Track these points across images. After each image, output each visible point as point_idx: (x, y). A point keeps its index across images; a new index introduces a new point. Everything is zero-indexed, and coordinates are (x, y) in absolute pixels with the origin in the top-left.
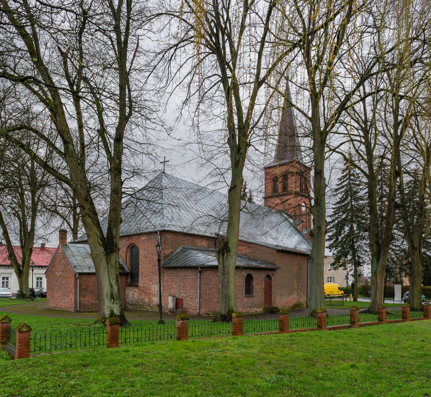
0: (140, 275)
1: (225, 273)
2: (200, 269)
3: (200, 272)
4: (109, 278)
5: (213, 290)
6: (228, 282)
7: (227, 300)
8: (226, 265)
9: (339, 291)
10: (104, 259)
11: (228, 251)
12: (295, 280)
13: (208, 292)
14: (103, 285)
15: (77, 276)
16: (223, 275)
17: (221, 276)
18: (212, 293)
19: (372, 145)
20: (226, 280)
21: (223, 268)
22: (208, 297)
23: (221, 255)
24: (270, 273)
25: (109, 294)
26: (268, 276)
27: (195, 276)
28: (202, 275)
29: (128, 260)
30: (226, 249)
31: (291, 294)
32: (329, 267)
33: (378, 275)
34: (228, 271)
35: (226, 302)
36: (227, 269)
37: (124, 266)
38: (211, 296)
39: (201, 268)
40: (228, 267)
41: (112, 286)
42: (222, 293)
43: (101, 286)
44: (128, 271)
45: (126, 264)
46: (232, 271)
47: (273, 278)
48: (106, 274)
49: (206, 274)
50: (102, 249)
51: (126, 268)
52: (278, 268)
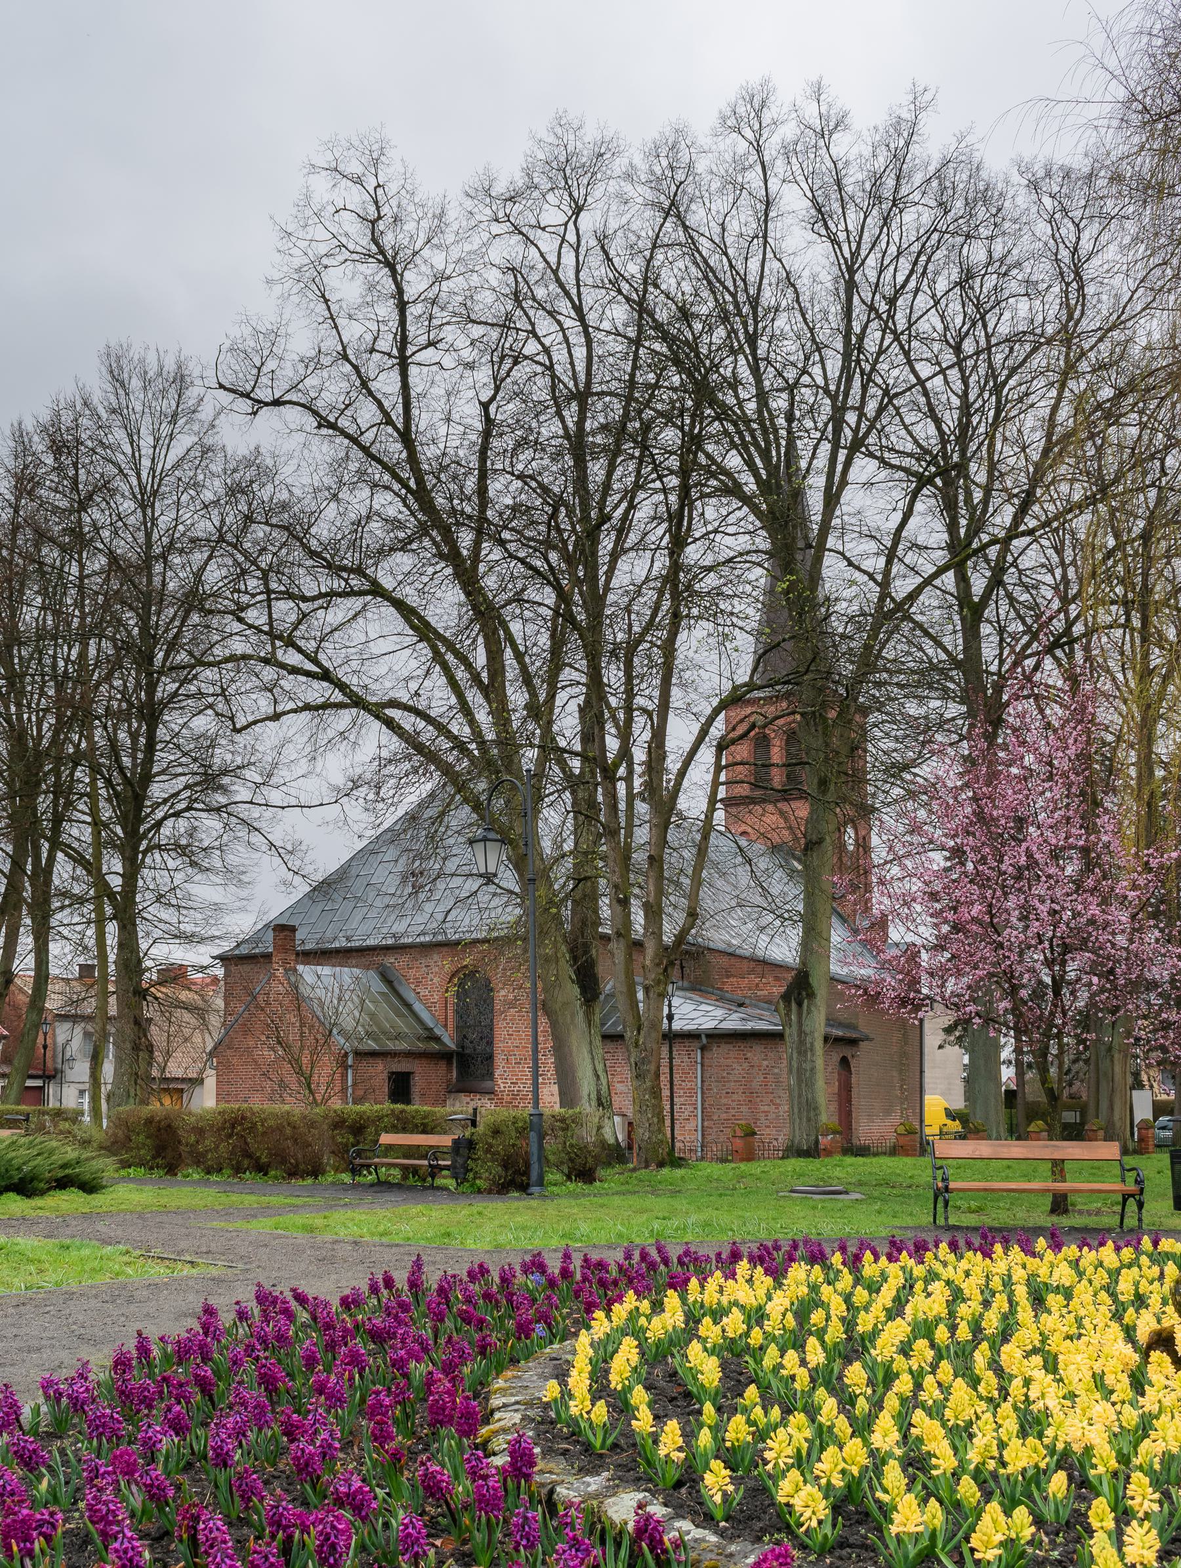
0: (499, 1060)
1: (803, 1049)
2: (704, 1040)
3: (703, 1049)
4: (593, 1059)
5: (735, 1097)
6: (813, 1069)
7: (812, 1114)
8: (807, 1029)
9: (949, 1122)
10: (581, 1015)
11: (811, 995)
12: (895, 1074)
13: (724, 1101)
14: (580, 1074)
15: (350, 1061)
16: (799, 1053)
17: (795, 1055)
18: (734, 1104)
19: (815, 501)
20: (807, 1066)
21: (799, 1035)
22: (724, 1116)
23: (794, 1006)
24: (847, 1052)
25: (594, 1096)
26: (845, 1062)
27: (686, 1059)
28: (708, 1054)
29: (450, 1014)
30: (805, 989)
31: (888, 1112)
32: (940, 1037)
33: (1116, 1056)
34: (812, 1044)
35: (809, 1120)
36: (808, 1039)
37: (438, 1031)
38: (733, 1112)
39: (708, 1036)
40: (812, 1032)
41: (598, 1077)
42: (800, 1096)
43: (574, 1077)
44: (453, 1047)
45: (445, 1026)
46: (819, 1044)
47: (853, 1063)
48: (585, 1051)
49: (720, 1053)
50: (576, 990)
51: (446, 1040)
52: (867, 1039)
